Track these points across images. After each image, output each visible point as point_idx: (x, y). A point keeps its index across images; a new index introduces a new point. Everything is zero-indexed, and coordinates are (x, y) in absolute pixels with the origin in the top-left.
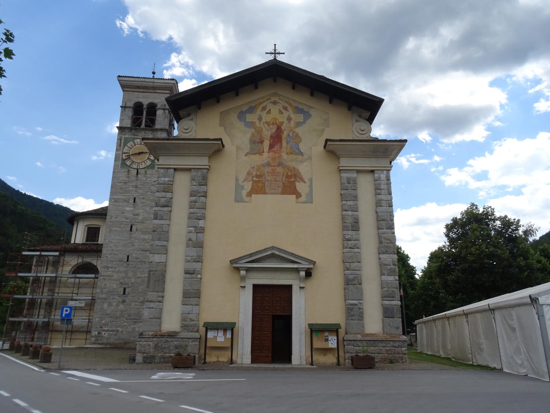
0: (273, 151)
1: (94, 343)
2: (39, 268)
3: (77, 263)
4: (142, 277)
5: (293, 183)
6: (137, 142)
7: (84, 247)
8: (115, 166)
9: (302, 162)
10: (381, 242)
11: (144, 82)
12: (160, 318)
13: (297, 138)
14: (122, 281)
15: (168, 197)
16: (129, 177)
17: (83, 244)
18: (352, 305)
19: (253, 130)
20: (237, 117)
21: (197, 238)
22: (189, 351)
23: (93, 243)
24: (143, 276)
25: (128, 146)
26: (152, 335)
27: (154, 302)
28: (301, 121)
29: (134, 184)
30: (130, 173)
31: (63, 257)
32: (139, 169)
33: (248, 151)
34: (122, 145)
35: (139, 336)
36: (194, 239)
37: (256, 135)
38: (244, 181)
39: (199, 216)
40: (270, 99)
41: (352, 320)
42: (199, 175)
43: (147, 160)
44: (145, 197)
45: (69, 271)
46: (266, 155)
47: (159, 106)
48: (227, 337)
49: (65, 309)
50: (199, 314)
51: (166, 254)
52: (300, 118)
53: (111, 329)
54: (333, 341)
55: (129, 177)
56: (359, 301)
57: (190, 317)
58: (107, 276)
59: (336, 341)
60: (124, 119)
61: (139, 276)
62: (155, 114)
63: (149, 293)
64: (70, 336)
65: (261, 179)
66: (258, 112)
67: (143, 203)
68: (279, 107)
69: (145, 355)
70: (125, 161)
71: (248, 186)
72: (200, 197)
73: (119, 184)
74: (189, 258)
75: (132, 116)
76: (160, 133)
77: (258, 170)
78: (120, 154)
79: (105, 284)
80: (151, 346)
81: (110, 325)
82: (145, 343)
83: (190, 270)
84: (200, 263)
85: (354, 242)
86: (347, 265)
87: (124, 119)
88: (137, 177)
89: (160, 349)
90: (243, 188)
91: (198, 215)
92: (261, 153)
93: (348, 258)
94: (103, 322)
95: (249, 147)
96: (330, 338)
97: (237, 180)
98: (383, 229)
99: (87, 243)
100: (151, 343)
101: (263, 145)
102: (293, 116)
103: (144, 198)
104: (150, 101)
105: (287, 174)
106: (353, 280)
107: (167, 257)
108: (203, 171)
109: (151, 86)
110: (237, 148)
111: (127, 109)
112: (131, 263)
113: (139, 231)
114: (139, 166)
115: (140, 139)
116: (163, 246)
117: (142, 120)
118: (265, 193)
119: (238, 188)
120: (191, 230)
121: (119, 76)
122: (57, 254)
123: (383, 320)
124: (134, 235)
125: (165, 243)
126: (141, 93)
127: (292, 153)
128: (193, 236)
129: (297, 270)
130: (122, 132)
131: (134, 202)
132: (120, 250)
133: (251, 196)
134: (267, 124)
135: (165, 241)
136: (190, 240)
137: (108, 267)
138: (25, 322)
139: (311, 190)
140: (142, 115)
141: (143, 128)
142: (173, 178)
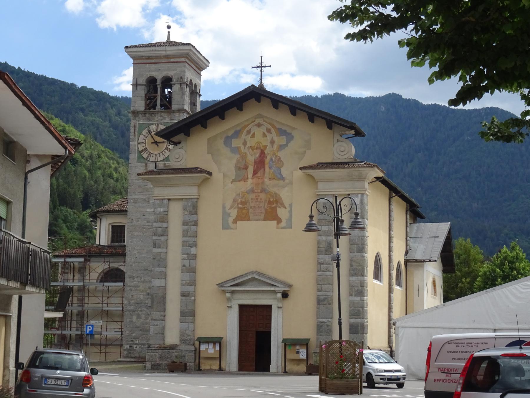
0: (257, 177)
1: (127, 357)
2: (66, 276)
3: (104, 270)
5: (274, 210)
6: (153, 129)
7: (110, 250)
9: (283, 187)
10: (351, 265)
12: (163, 334)
13: (280, 163)
14: (148, 291)
15: (164, 227)
17: (108, 246)
18: (321, 322)
19: (238, 156)
20: (223, 142)
21: (189, 264)
22: (187, 360)
25: (143, 135)
26: (157, 347)
27: (158, 320)
28: (284, 144)
30: (147, 168)
31: (89, 263)
32: (157, 162)
33: (234, 178)
34: (137, 133)
35: (147, 348)
36: (187, 265)
37: (241, 161)
38: (230, 209)
39: (191, 244)
40: (255, 121)
41: (321, 335)
42: (190, 204)
43: (166, 151)
46: (250, 181)
48: (216, 349)
49: (88, 327)
50: (194, 330)
51: (165, 279)
52: (282, 140)
53: (142, 342)
54: (303, 353)
56: (328, 319)
57: (186, 333)
58: (133, 287)
59: (306, 354)
60: (136, 101)
63: (153, 313)
64: (105, 349)
65: (246, 206)
66: (243, 136)
68: (263, 129)
69: (153, 363)
70: (142, 154)
71: (234, 213)
72: (191, 226)
73: (137, 182)
74: (184, 282)
76: (178, 115)
77: (243, 197)
78: (135, 145)
79: (132, 296)
80: (157, 356)
81: (140, 338)
82: (152, 354)
83: (185, 293)
84: (193, 287)
85: (326, 265)
86: (320, 287)
87: (136, 101)
89: (164, 359)
90: (229, 215)
91: (191, 243)
92: (245, 179)
93: (320, 281)
94: (134, 335)
95: (235, 173)
96: (301, 351)
97: (224, 208)
98: (354, 252)
100: (157, 354)
101: (247, 172)
102: (276, 139)
104: (164, 74)
105: (269, 199)
106: (324, 300)
107: (166, 281)
108: (193, 200)
110: (224, 175)
114: (156, 159)
115: (155, 124)
117: (157, 99)
118: (249, 220)
119: (225, 215)
120: (184, 257)
121: (127, 47)
122: (82, 260)
123: (349, 336)
125: (163, 269)
127: (274, 179)
128: (187, 263)
129: (275, 292)
133: (237, 223)
134: (251, 149)
135: (164, 267)
136: (184, 266)
137: (134, 277)
138: (58, 335)
139: (291, 216)
142: (168, 208)
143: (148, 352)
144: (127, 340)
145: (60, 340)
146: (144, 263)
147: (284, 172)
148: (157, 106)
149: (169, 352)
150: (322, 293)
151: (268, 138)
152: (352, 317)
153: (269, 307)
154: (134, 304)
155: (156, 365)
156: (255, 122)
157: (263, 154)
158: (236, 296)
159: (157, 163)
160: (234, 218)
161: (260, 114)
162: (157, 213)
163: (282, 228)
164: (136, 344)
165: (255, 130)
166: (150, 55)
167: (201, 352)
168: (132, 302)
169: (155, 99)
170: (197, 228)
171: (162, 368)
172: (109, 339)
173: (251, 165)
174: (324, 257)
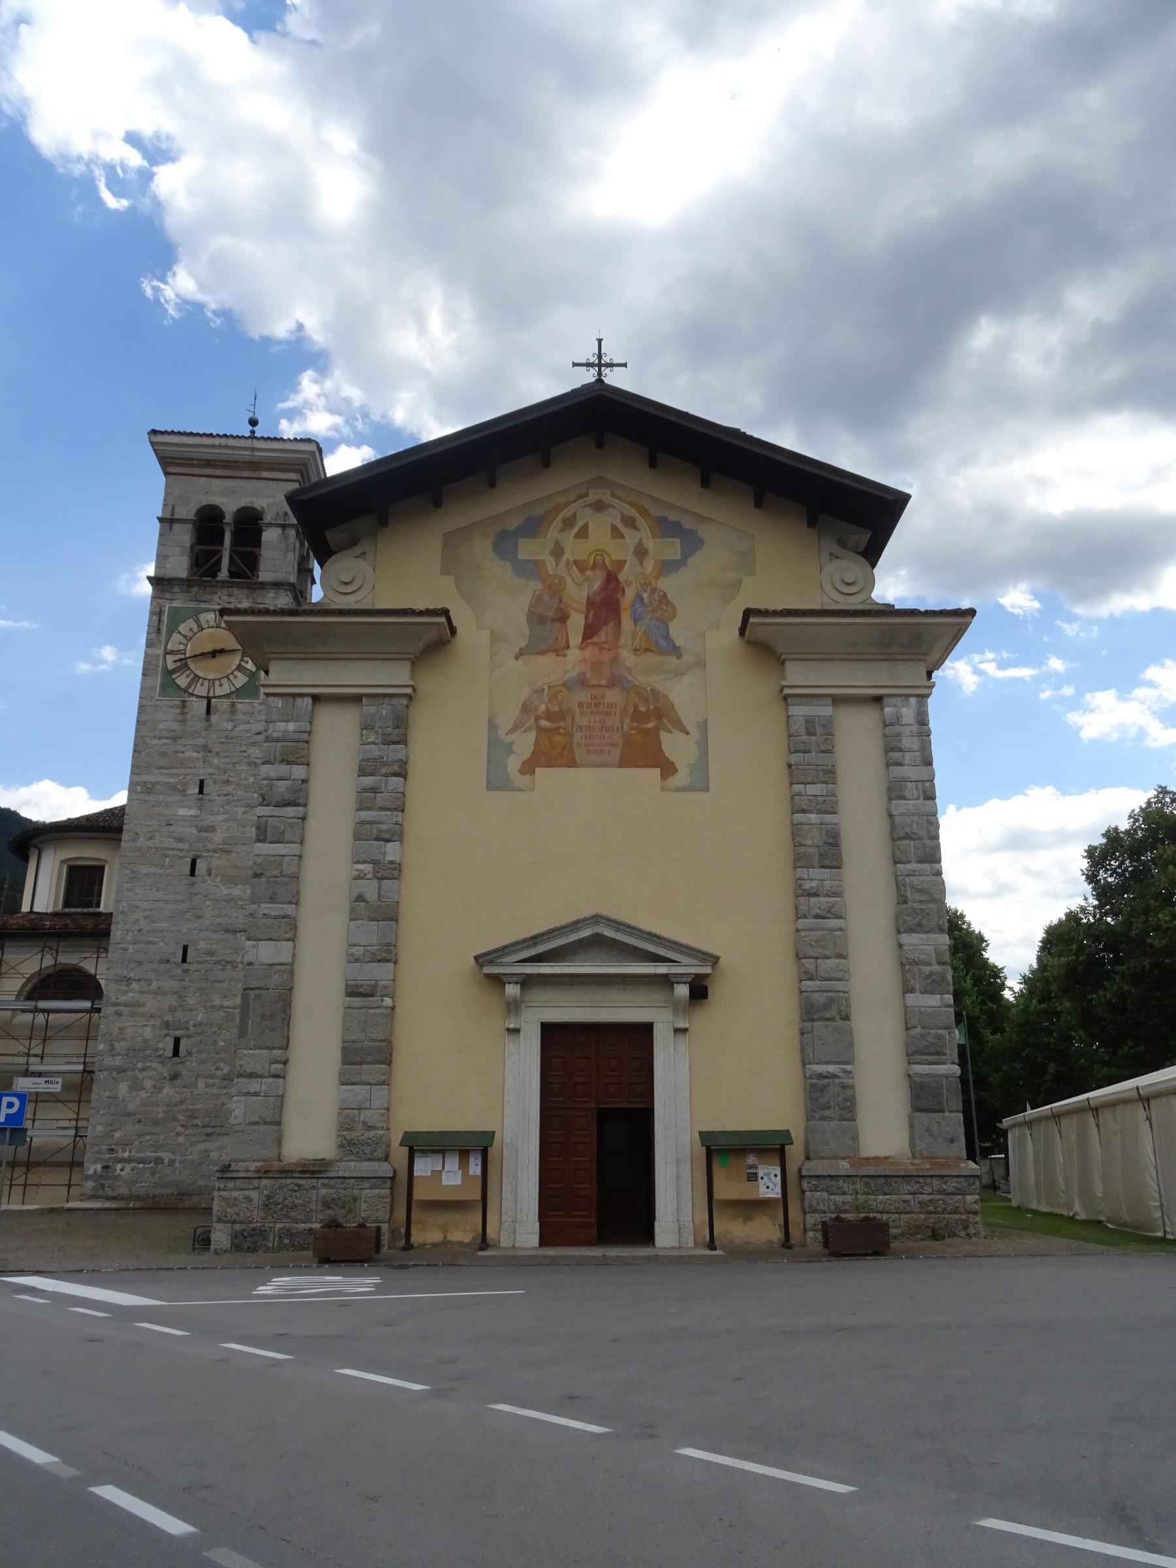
0: (595, 644)
1: (94, 1197)
4: (228, 1007)
5: (653, 737)
6: (207, 621)
8: (142, 689)
10: (902, 900)
11: (226, 447)
12: (279, 1123)
13: (665, 607)
14: (168, 1018)
15: (296, 777)
16: (183, 722)
17: (55, 915)
18: (821, 1076)
19: (537, 585)
20: (490, 547)
23: (86, 910)
24: (229, 1003)
25: (180, 633)
29: (200, 741)
30: (186, 710)
32: (214, 697)
33: (524, 644)
34: (164, 629)
35: (218, 1175)
38: (513, 730)
40: (587, 495)
41: (823, 1118)
42: (384, 712)
43: (237, 673)
44: (231, 779)
45: (16, 993)
46: (574, 654)
47: (269, 517)
48: (471, 1173)
50: (388, 1109)
52: (672, 549)
53: (141, 1155)
54: (770, 1178)
55: (183, 722)
56: (843, 1067)
57: (362, 1118)
61: (217, 1001)
62: (257, 542)
63: (246, 1052)
65: (562, 724)
67: (227, 795)
68: (611, 518)
69: (237, 1227)
70: (174, 676)
71: (525, 744)
72: (386, 775)
73: (156, 742)
74: (358, 951)
75: (192, 547)
77: (553, 697)
78: (158, 656)
80: (255, 1202)
81: (137, 1143)
82: (235, 1194)
85: (827, 899)
87: (168, 556)
88: (208, 720)
89: (282, 1209)
90: (509, 749)
91: (384, 827)
92: (560, 649)
94: (117, 1135)
97: (492, 726)
98: (909, 862)
99: (67, 910)
100: (254, 1195)
102: (650, 544)
103: (227, 782)
104: (244, 502)
105: (636, 707)
106: (826, 1006)
107: (295, 947)
108: (395, 701)
109: (248, 459)
111: (177, 527)
112: (195, 967)
113: (216, 876)
115: (214, 611)
116: (284, 917)
118: (572, 763)
119: (497, 748)
120: (362, 871)
124: (200, 888)
125: (289, 909)
126: (218, 482)
127: (647, 650)
128: (370, 889)
129: (667, 982)
130: (163, 591)
131: (201, 792)
132: (161, 931)
133: (534, 772)
134: (577, 567)
135: (290, 903)
136: (360, 898)
137: (129, 979)
139: (704, 755)
140: (222, 543)
141: (223, 579)
142: (311, 723)
143: (219, 1190)
144: (95, 1148)
145: (1151, 817)
146: (161, 944)
147: (678, 631)
148: (220, 571)
149: (300, 1186)
150: (818, 983)
151: (628, 540)
152: (918, 1058)
153: (645, 1031)
154: (124, 1052)
155: (252, 1236)
156: (585, 499)
157: (612, 580)
158: (539, 996)
159: (213, 700)
160: (525, 760)
161: (600, 478)
162: (275, 735)
163: (677, 790)
164: (123, 1160)
165: (586, 517)
166: (210, 457)
167: (415, 1182)
168: (120, 1046)
169: (218, 556)
170: (404, 786)
171: (270, 1244)
172: (38, 1149)
173: (577, 611)
174: (817, 873)
